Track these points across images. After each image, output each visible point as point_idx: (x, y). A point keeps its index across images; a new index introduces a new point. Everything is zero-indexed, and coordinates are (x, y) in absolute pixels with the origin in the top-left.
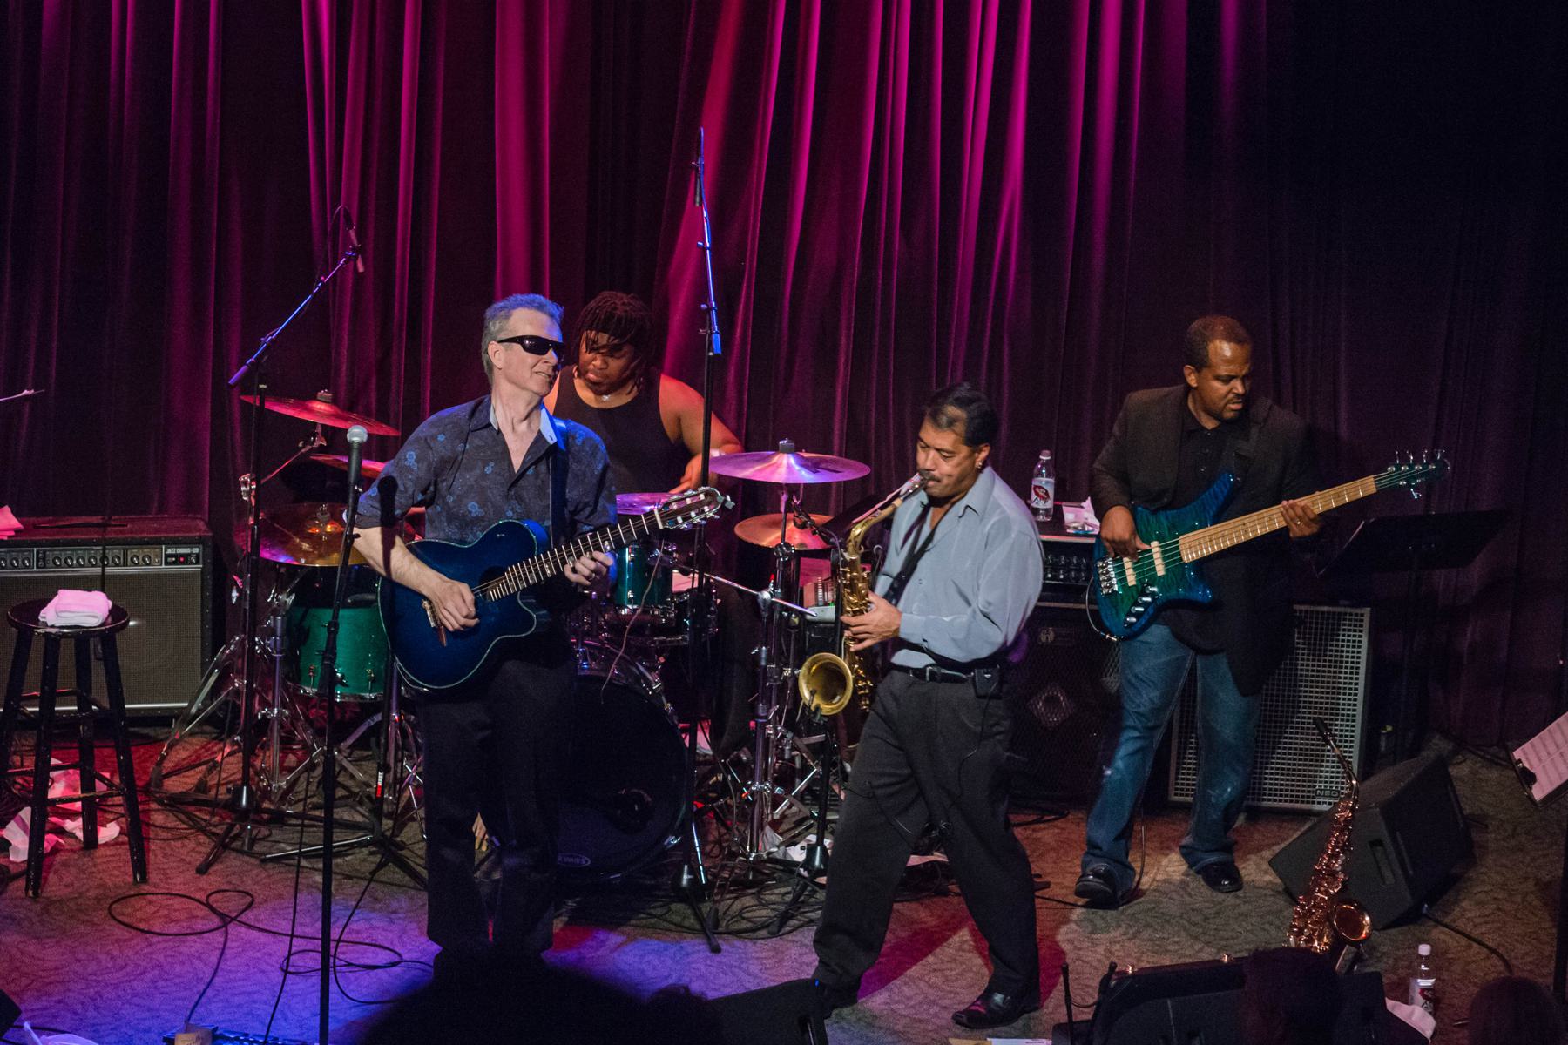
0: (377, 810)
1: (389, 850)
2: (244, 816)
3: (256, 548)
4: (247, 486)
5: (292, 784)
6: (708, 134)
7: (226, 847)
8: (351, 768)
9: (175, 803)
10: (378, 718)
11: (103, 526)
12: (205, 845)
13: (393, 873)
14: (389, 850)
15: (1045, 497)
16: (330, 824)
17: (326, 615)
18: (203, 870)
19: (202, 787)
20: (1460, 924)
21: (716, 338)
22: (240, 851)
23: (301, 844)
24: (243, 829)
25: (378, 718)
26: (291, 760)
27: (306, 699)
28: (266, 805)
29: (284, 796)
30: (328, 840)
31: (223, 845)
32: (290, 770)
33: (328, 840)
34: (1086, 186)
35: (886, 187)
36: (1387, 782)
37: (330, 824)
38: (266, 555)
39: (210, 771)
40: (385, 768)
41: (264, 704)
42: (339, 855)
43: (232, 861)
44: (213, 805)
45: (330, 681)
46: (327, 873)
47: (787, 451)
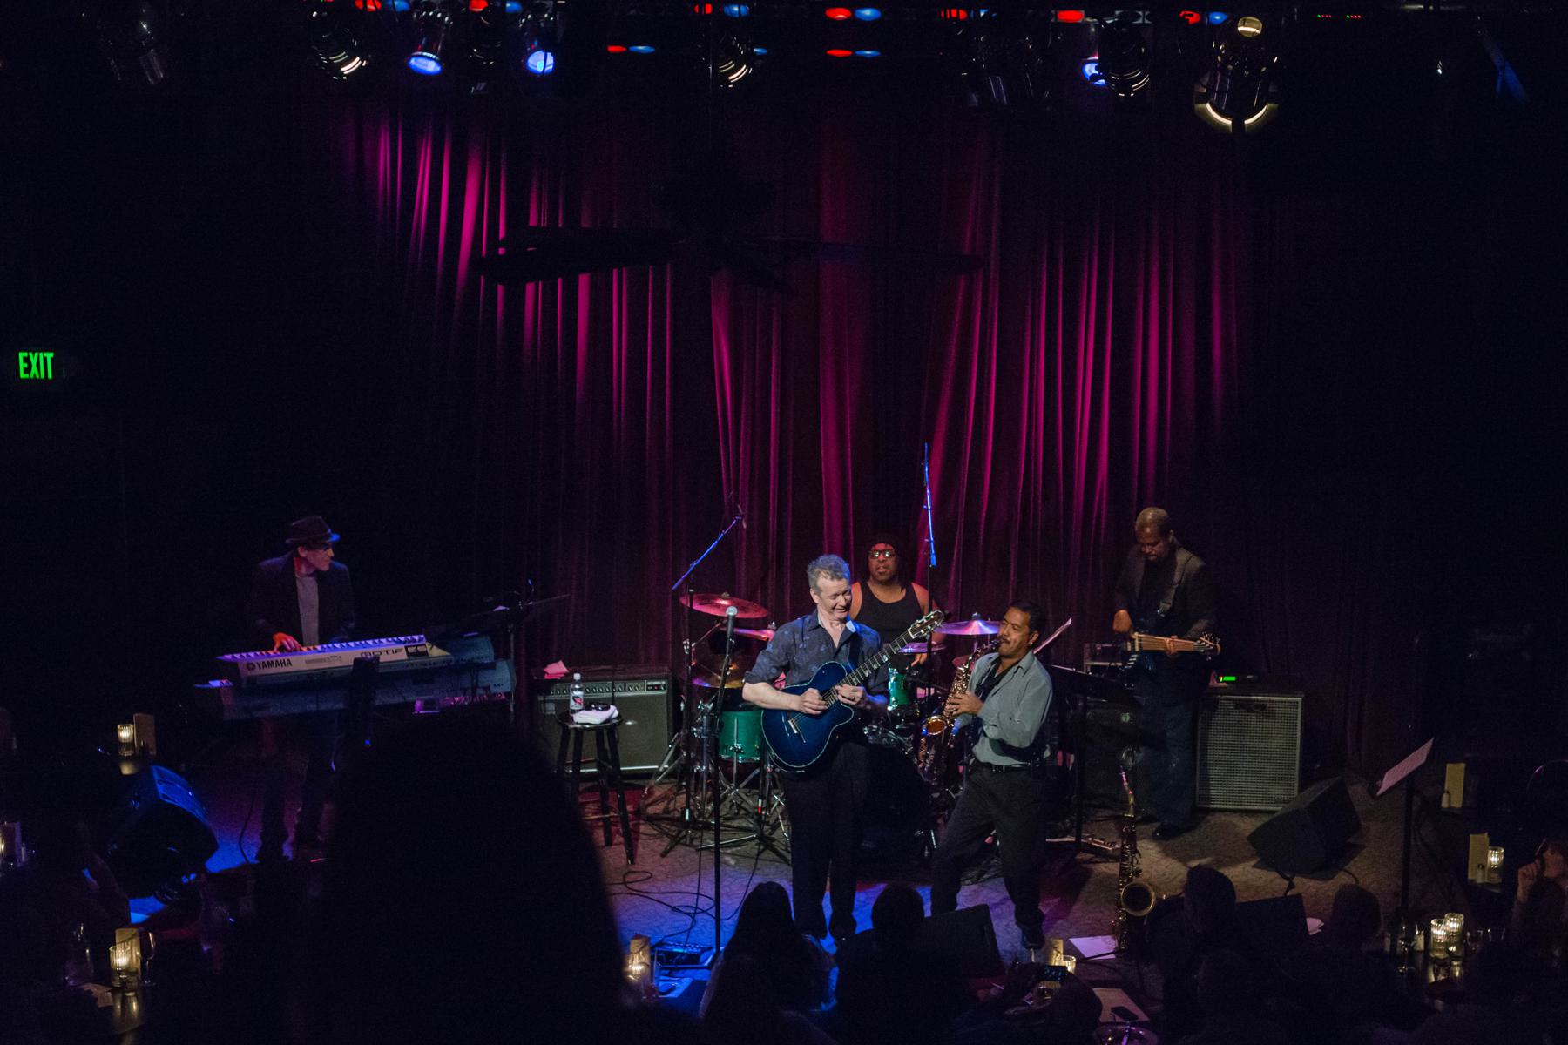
0: (760, 821)
1: (766, 842)
2: (686, 825)
3: (690, 679)
4: (688, 645)
7: (678, 843)
9: (652, 820)
11: (613, 671)
12: (666, 841)
13: (768, 854)
14: (766, 842)
16: (717, 818)
18: (664, 854)
19: (667, 811)
20: (1353, 870)
31: (676, 841)
34: (1143, 441)
35: (1026, 406)
36: (1315, 792)
38: (696, 682)
40: (762, 797)
43: (680, 849)
44: (673, 821)
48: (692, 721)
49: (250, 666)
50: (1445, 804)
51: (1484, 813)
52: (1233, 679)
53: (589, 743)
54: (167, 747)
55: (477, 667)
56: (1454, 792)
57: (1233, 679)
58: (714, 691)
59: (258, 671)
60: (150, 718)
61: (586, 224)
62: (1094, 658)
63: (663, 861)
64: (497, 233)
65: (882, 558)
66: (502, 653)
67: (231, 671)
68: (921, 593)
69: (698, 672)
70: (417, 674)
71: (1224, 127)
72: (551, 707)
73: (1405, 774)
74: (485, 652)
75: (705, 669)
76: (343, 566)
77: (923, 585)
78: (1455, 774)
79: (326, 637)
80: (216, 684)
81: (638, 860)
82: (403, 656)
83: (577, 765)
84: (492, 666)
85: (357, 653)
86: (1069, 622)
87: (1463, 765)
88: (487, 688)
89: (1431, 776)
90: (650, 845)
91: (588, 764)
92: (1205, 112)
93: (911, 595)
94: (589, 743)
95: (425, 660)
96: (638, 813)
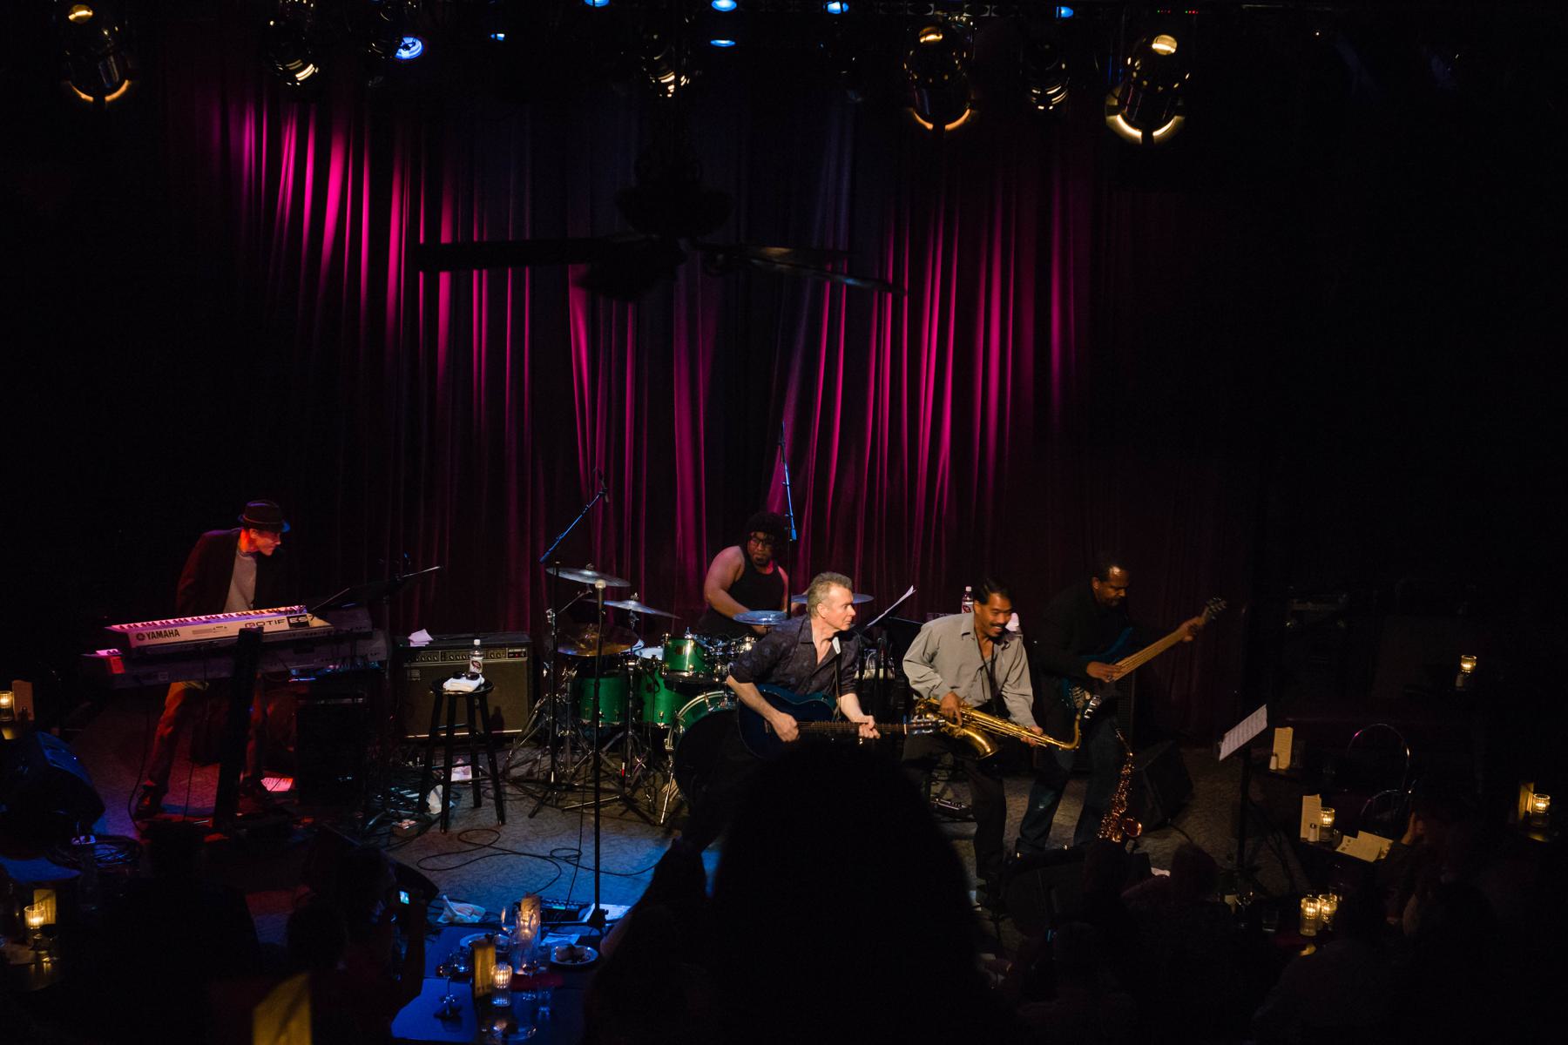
2: (552, 787)
4: (551, 614)
6: (787, 424)
9: (516, 782)
13: (631, 815)
17: (593, 681)
19: (530, 773)
21: (794, 533)
31: (542, 802)
35: (872, 394)
38: (561, 650)
40: (626, 761)
43: (547, 811)
44: (537, 782)
45: (596, 717)
46: (597, 816)
48: (556, 688)
49: (140, 637)
50: (1273, 766)
51: (1308, 774)
53: (462, 707)
54: (573, 681)
55: (355, 637)
56: (1282, 755)
59: (147, 642)
60: (28, 685)
61: (445, 238)
64: (438, 233)
66: (377, 624)
67: (121, 640)
69: (562, 640)
70: (298, 643)
71: (1133, 139)
72: (417, 673)
73: (1256, 732)
74: (363, 621)
78: (1284, 740)
79: (259, 603)
80: (103, 653)
82: (285, 626)
83: (450, 730)
84: (368, 636)
85: (242, 624)
86: (911, 591)
87: (1290, 730)
88: (364, 658)
89: (1264, 741)
90: (518, 808)
91: (460, 729)
92: (1115, 124)
94: (462, 707)
95: (304, 630)
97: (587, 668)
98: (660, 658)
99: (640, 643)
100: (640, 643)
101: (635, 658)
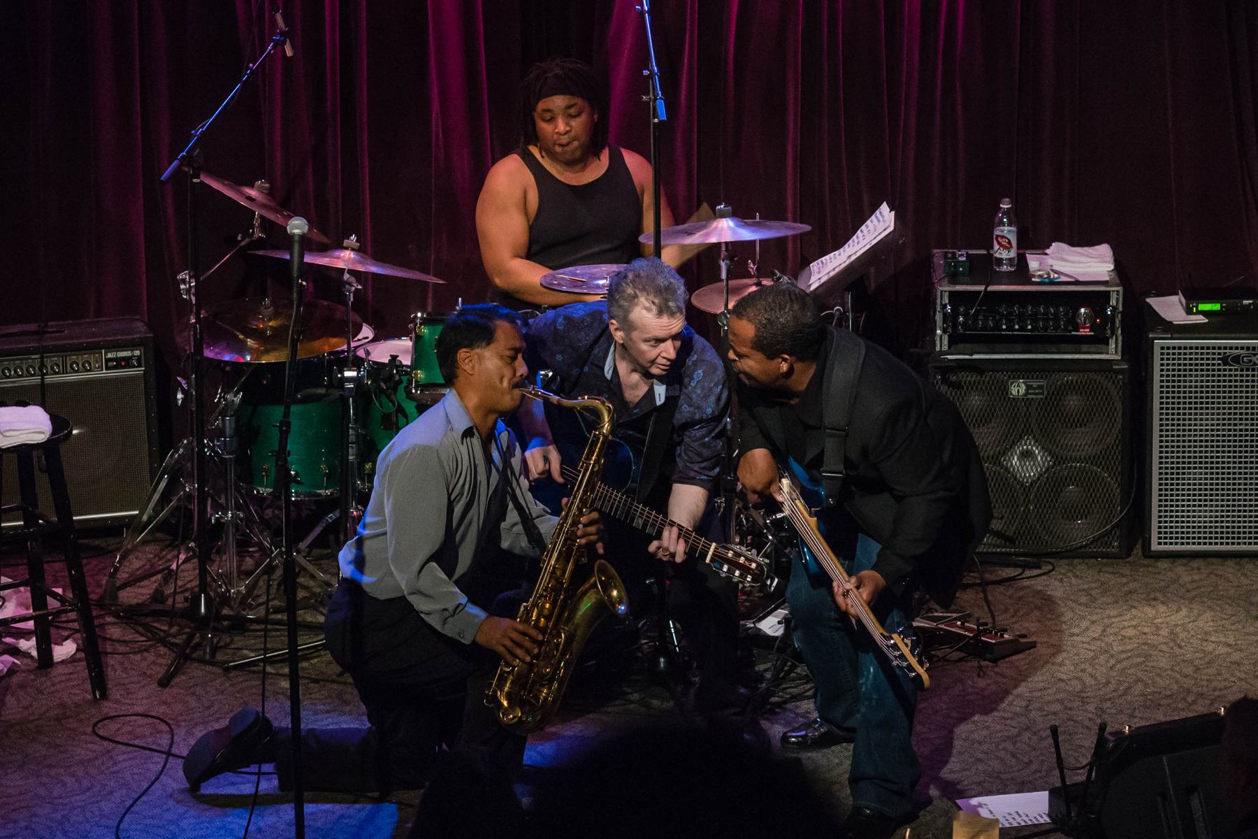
2: (202, 624)
4: (186, 282)
5: (251, 588)
7: (187, 658)
8: (310, 567)
9: (131, 615)
10: (331, 517)
11: (40, 334)
15: (1008, 247)
18: (164, 682)
19: (158, 596)
22: (201, 661)
23: (266, 650)
24: (204, 637)
25: (331, 517)
26: (249, 562)
27: (260, 499)
28: (225, 611)
29: (243, 602)
30: (293, 643)
31: (184, 656)
32: (248, 574)
33: (293, 643)
37: (294, 627)
38: (209, 353)
39: (166, 580)
41: (217, 507)
42: (306, 658)
43: (196, 671)
45: (284, 481)
46: (294, 678)
47: (723, 215)
52: (1216, 307)
57: (1216, 307)
58: (239, 367)
62: (954, 278)
63: (167, 693)
65: (562, 120)
68: (637, 167)
69: (213, 332)
75: (225, 321)
76: (606, 427)
77: (644, 153)
81: (115, 693)
93: (617, 169)
96: (108, 602)
97: (262, 386)
98: (406, 361)
99: (367, 332)
100: (367, 332)
101: (357, 363)
